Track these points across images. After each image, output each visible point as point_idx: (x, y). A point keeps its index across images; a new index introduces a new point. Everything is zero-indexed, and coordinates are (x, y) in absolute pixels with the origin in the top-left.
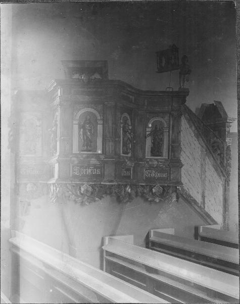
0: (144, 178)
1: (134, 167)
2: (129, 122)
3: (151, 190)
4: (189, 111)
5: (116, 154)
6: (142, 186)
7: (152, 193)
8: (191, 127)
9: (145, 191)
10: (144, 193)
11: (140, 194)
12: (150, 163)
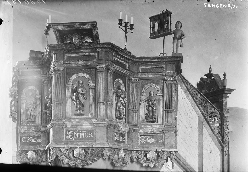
0: (139, 144)
1: (128, 133)
2: (122, 87)
3: (146, 156)
4: (185, 81)
5: (107, 116)
6: (137, 151)
7: (147, 159)
8: (187, 97)
9: (140, 157)
10: (139, 158)
11: (135, 160)
12: (144, 129)
